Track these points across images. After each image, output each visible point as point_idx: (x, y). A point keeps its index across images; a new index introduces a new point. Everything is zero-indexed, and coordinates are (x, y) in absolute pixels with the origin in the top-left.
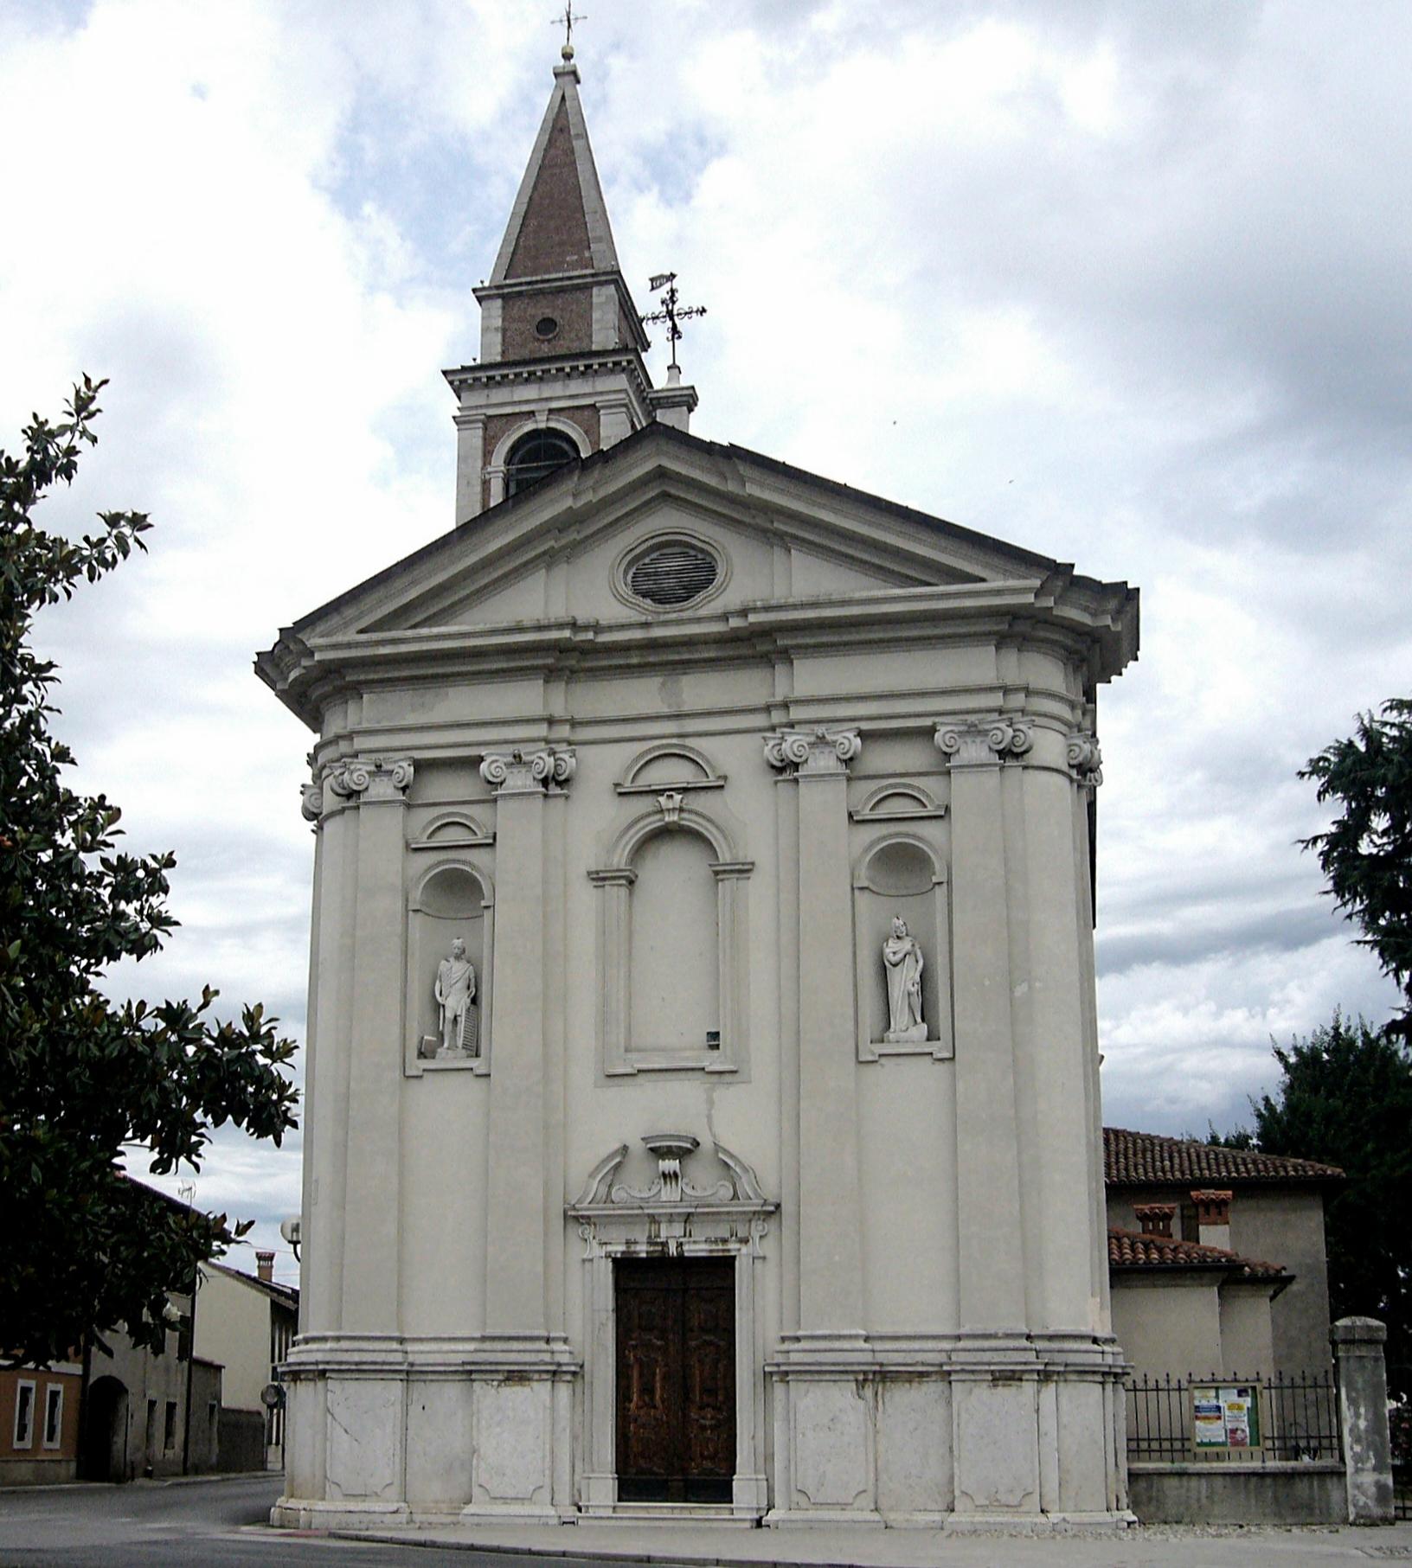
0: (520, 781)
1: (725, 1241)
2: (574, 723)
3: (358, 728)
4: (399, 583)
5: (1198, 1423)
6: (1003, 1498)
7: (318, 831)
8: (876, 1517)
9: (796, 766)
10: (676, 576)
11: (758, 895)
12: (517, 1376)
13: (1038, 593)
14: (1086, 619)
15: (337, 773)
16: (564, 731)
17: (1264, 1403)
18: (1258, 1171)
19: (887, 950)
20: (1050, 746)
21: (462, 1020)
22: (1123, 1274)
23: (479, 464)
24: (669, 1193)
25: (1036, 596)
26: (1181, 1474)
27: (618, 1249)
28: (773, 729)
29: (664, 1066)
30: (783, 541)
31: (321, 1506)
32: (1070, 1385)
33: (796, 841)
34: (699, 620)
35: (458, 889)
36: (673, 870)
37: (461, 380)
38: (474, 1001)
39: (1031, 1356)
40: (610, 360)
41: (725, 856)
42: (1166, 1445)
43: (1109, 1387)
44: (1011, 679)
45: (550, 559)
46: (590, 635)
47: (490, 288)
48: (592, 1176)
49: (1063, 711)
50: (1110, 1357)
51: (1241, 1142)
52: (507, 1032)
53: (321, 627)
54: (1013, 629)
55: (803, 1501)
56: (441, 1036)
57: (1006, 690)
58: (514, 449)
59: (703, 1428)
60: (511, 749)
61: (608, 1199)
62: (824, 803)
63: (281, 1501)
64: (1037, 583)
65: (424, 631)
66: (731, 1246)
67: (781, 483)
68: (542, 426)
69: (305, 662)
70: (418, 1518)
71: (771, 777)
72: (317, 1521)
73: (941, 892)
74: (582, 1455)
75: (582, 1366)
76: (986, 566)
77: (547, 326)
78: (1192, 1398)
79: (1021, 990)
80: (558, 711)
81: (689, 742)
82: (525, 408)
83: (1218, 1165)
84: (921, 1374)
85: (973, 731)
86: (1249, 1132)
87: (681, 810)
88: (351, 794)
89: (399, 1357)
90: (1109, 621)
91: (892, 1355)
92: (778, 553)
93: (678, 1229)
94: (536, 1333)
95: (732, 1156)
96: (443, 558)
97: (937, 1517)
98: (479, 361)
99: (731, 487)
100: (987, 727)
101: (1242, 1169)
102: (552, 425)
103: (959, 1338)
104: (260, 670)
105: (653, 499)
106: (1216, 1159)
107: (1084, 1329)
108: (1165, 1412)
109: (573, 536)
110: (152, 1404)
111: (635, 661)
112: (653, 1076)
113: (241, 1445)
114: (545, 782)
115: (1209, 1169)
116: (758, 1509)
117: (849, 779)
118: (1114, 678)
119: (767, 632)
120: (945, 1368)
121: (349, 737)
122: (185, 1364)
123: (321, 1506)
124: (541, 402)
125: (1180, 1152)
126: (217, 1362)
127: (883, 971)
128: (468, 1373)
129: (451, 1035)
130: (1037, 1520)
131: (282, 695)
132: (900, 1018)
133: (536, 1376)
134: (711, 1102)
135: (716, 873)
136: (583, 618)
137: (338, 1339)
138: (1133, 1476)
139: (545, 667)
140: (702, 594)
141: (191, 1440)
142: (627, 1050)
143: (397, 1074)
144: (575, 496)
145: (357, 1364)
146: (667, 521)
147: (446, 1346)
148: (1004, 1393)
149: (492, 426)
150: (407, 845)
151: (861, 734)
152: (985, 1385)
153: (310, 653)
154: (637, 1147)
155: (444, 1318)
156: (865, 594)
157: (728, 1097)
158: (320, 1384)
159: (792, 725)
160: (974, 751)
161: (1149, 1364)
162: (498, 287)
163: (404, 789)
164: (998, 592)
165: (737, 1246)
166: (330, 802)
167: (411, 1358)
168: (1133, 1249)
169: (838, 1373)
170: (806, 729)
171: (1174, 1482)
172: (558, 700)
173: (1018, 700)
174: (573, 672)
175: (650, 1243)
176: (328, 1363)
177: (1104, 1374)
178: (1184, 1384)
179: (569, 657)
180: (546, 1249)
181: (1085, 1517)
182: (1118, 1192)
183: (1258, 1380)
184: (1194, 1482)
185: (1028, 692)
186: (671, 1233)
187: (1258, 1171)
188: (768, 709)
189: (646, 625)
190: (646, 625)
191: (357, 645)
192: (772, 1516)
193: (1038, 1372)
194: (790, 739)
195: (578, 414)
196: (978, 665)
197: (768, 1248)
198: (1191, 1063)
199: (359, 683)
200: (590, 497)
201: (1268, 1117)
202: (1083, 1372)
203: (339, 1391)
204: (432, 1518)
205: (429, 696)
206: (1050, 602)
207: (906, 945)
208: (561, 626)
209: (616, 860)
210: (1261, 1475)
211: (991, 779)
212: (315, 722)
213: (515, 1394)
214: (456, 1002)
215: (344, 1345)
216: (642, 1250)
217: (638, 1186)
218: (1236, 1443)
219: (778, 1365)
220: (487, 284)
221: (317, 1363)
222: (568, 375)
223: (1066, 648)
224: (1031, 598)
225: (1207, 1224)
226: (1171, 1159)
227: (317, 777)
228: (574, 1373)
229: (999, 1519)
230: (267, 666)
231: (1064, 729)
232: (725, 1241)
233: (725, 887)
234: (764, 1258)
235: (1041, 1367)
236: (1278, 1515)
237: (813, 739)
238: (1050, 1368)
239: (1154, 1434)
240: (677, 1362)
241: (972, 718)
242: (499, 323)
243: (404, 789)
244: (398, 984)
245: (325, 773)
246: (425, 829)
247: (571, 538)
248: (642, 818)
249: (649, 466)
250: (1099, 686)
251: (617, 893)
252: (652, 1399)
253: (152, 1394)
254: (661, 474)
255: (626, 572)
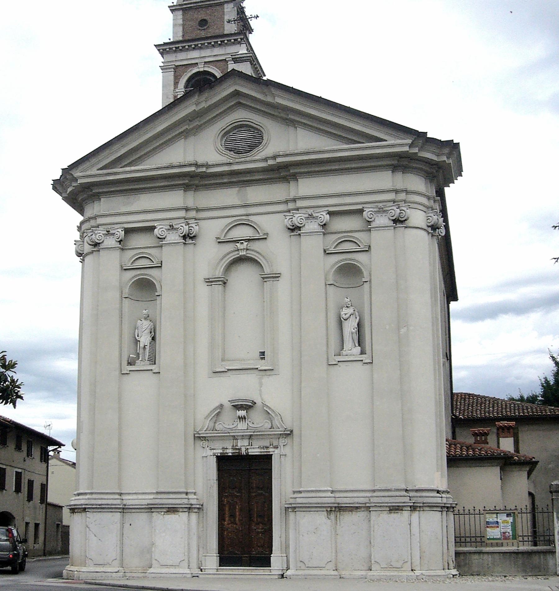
0: (174, 237)
1: (267, 448)
2: (198, 210)
3: (99, 214)
4: (115, 147)
5: (488, 529)
6: (395, 564)
7: (82, 261)
8: (335, 573)
9: (299, 228)
10: (245, 139)
11: (282, 288)
12: (172, 510)
13: (411, 146)
14: (435, 158)
15: (89, 235)
16: (193, 214)
17: (519, 520)
18: (533, 412)
19: (342, 313)
20: (418, 217)
21: (148, 347)
22: (453, 461)
23: (172, 88)
24: (242, 426)
25: (410, 147)
26: (480, 553)
27: (219, 452)
28: (289, 211)
29: (241, 367)
30: (293, 123)
31: (84, 569)
32: (425, 512)
33: (300, 263)
34: (255, 161)
35: (145, 287)
36: (244, 277)
37: (164, 49)
38: (153, 339)
39: (407, 499)
40: (232, 39)
41: (267, 270)
42: (473, 539)
43: (445, 513)
44: (399, 186)
45: (186, 134)
46: (204, 169)
47: (176, 6)
48: (206, 418)
49: (424, 200)
50: (445, 499)
51: (533, 399)
52: (167, 352)
53: (81, 168)
54: (400, 163)
55: (303, 567)
56: (138, 354)
57: (397, 191)
58: (189, 81)
59: (258, 533)
60: (168, 223)
61: (214, 429)
62: (312, 244)
63: (68, 567)
64: (409, 141)
65: (128, 169)
66: (271, 450)
67: (292, 97)
68: (202, 70)
69: (74, 184)
70: (128, 575)
71: (288, 233)
72: (83, 576)
73: (366, 286)
74: (202, 546)
75: (202, 505)
76: (387, 134)
77: (203, 23)
78: (485, 518)
79: (403, 331)
80: (190, 204)
81: (251, 218)
82: (193, 62)
83: (514, 410)
84: (357, 508)
85: (381, 211)
86: (537, 394)
87: (247, 249)
88: (96, 245)
89: (118, 502)
90: (445, 158)
91: (345, 500)
92: (291, 129)
93: (246, 442)
94: (182, 490)
95: (270, 408)
96: (136, 134)
97: (363, 573)
98: (172, 40)
99: (269, 99)
100: (388, 209)
101: (526, 411)
102: (206, 69)
103: (374, 491)
104: (55, 188)
105: (233, 106)
106: (514, 407)
107: (433, 487)
108: (472, 525)
109: (196, 123)
110: (27, 524)
111: (225, 181)
112: (234, 372)
113: (58, 543)
114: (184, 237)
115: (510, 412)
116: (282, 570)
117: (324, 234)
118: (451, 185)
119: (286, 166)
120: (367, 505)
121: (95, 218)
122: (44, 505)
123: (84, 569)
124: (201, 58)
125: (498, 404)
126: (61, 505)
127: (340, 323)
128: (151, 509)
129: (142, 355)
130: (410, 574)
131: (65, 199)
132: (348, 344)
133: (181, 510)
134: (261, 384)
135: (263, 278)
136: (200, 161)
137: (92, 493)
138: (457, 554)
139: (184, 184)
140: (256, 150)
141: (47, 540)
142: (223, 360)
143: (117, 373)
144: (197, 105)
145: (99, 505)
146: (240, 115)
147: (140, 497)
148: (394, 516)
149: (178, 70)
150: (122, 267)
151: (330, 213)
152: (386, 512)
153: (76, 180)
154: (227, 405)
155: (140, 484)
156: (335, 147)
157: (269, 381)
158: (83, 514)
159: (297, 209)
160: (382, 220)
161: (467, 502)
162: (180, 5)
163: (120, 242)
164: (393, 146)
165: (273, 450)
166: (87, 248)
167: (125, 502)
168: (461, 449)
169: (318, 507)
170: (303, 211)
171: (476, 557)
172: (191, 199)
173: (402, 196)
174: (197, 186)
175: (233, 449)
176: (87, 505)
177: (442, 507)
178: (482, 512)
179: (195, 179)
180: (185, 452)
181: (432, 573)
182: (456, 424)
183: (516, 509)
184: (486, 556)
185: (407, 192)
186: (242, 444)
187: (533, 412)
188: (286, 202)
189: (230, 164)
190: (230, 164)
191: (100, 175)
192: (289, 573)
193: (411, 507)
194: (297, 216)
195: (219, 63)
196: (384, 180)
197: (287, 451)
198: (527, 360)
199: (99, 193)
200: (204, 105)
201: (546, 386)
202: (432, 507)
203: (92, 517)
204: (134, 575)
205: (132, 198)
206: (416, 150)
207: (350, 311)
208: (190, 165)
209: (217, 273)
210: (517, 553)
211: (389, 234)
212: (81, 211)
213: (172, 518)
214: (145, 339)
215: (94, 496)
216: (230, 452)
217: (229, 422)
218: (505, 538)
219: (291, 504)
220: (175, 4)
221: (82, 505)
222: (213, 46)
223: (426, 172)
224: (406, 149)
225: (503, 437)
226: (493, 407)
227: (82, 237)
228: (199, 508)
229: (392, 574)
230: (58, 186)
231: (425, 209)
232: (267, 448)
233: (268, 285)
234: (285, 455)
235: (412, 504)
236: (525, 571)
237: (307, 216)
238: (415, 505)
239: (463, 535)
240: (244, 504)
241: (380, 205)
242: (181, 22)
243: (120, 242)
244: (373, 320)
245: (85, 234)
246: (129, 261)
247: (197, 124)
248: (228, 254)
249: (231, 90)
250: (445, 188)
251: (218, 288)
252: (235, 520)
253: (27, 519)
254: (237, 93)
255: (221, 140)
